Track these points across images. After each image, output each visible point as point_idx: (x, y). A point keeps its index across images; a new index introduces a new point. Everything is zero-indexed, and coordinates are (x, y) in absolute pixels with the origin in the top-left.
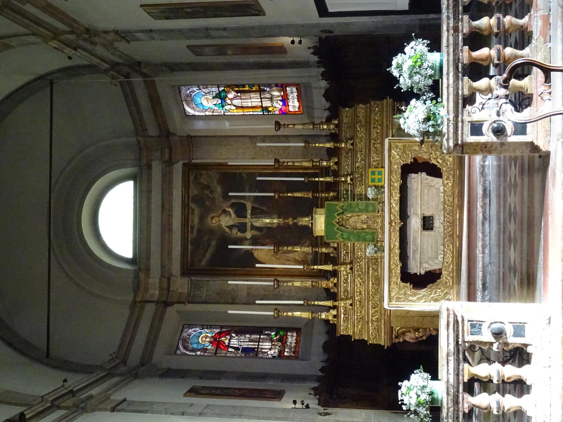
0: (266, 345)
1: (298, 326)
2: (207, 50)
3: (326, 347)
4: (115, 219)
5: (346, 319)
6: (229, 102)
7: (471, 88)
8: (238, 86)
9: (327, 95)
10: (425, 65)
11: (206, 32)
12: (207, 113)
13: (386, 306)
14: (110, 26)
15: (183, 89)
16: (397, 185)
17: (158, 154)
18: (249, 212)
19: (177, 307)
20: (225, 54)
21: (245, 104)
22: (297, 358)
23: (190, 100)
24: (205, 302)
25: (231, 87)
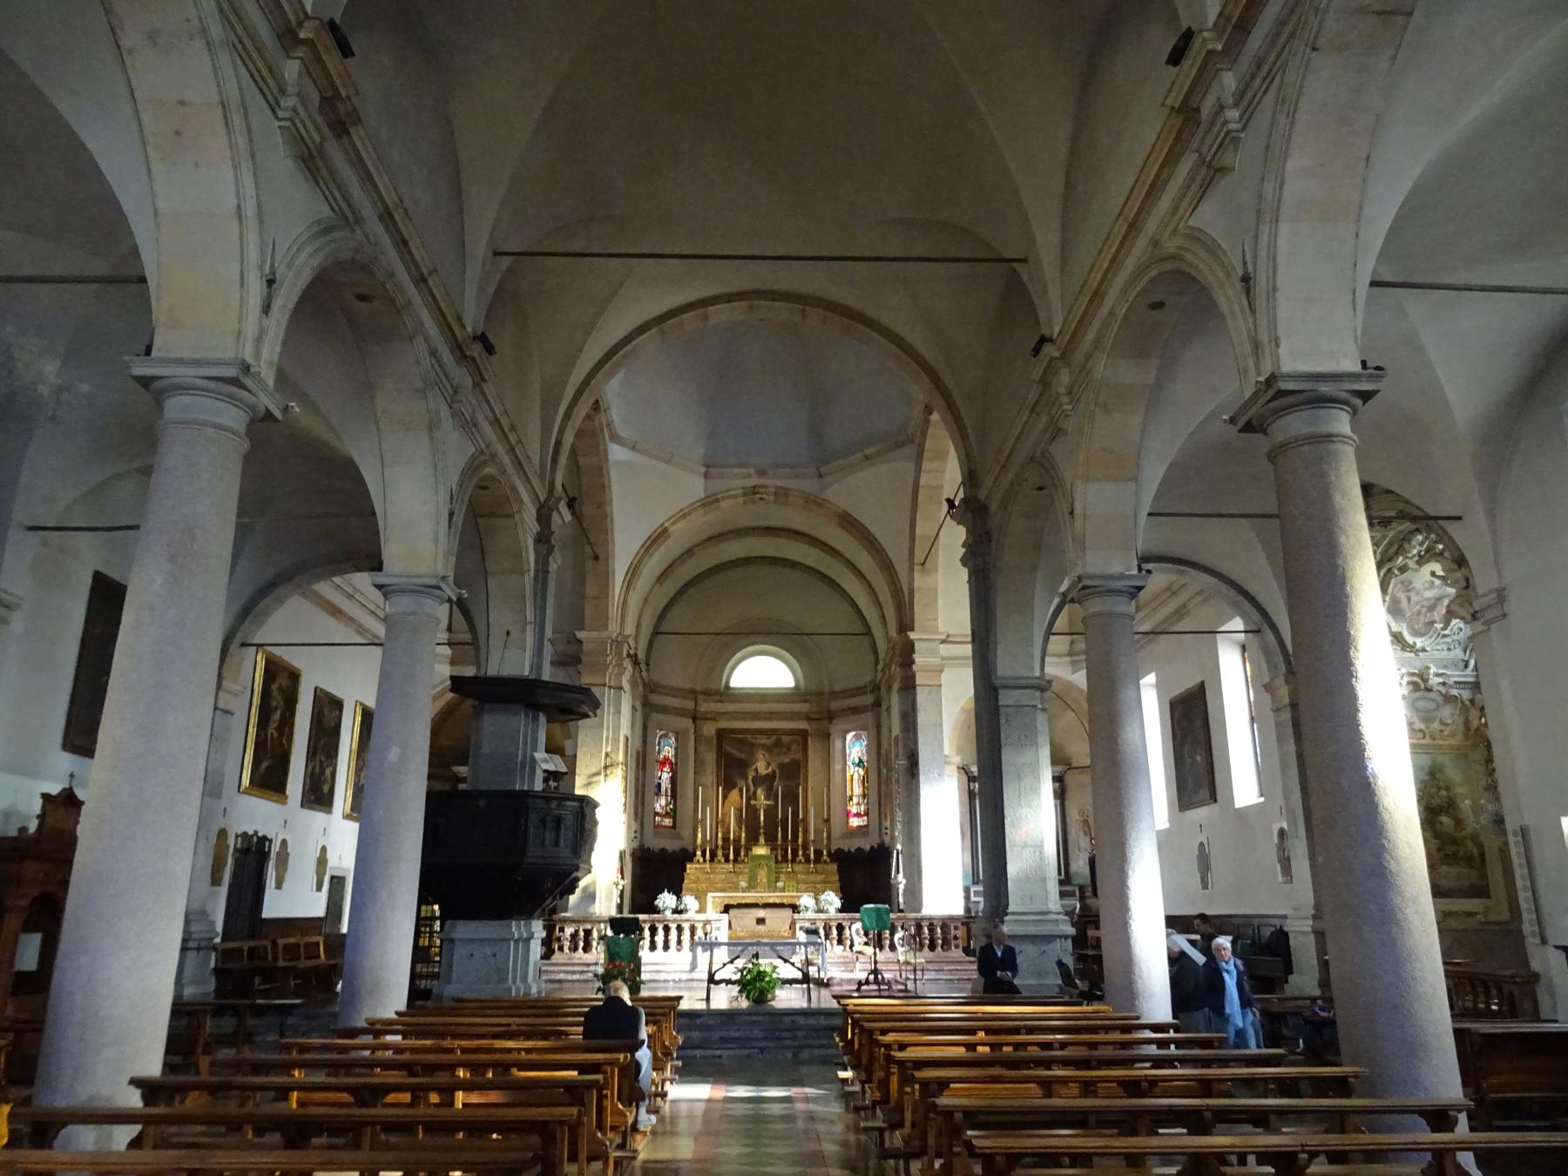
0: (663, 801)
3: (663, 850)
4: (762, 672)
9: (859, 850)
23: (857, 737)
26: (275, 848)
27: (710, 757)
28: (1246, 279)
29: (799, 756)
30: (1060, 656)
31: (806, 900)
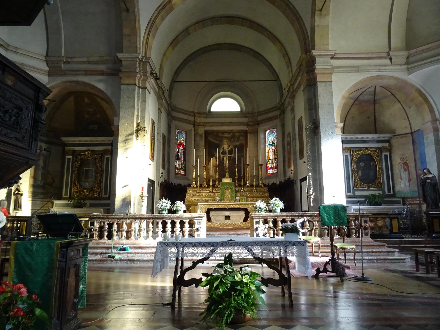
0: (180, 163)
1: (187, 175)
2: (289, 139)
3: (180, 185)
4: (226, 104)
5: (193, 191)
6: (271, 147)
7: (270, 221)
8: (277, 150)
9: (274, 184)
10: (276, 207)
11: (294, 139)
12: (266, 139)
13: (199, 203)
14: (296, 105)
15: (275, 130)
16: (241, 207)
17: (251, 120)
18: (230, 156)
19: (193, 129)
20: (288, 145)
21: (270, 153)
22: (175, 174)
23: (271, 132)
24: (195, 139)
25: (276, 148)
27: (202, 143)
30: (401, 65)
31: (261, 204)
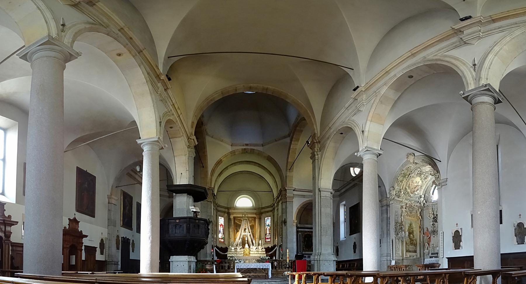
26: (131, 242)
28: (363, 131)
29: (254, 224)
